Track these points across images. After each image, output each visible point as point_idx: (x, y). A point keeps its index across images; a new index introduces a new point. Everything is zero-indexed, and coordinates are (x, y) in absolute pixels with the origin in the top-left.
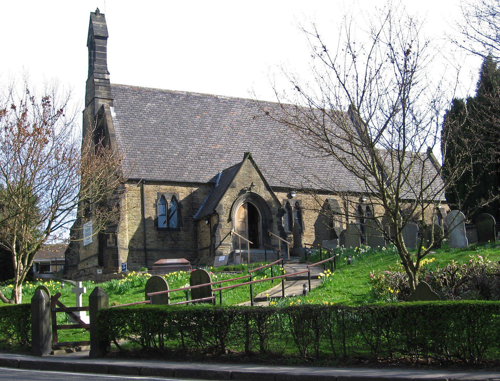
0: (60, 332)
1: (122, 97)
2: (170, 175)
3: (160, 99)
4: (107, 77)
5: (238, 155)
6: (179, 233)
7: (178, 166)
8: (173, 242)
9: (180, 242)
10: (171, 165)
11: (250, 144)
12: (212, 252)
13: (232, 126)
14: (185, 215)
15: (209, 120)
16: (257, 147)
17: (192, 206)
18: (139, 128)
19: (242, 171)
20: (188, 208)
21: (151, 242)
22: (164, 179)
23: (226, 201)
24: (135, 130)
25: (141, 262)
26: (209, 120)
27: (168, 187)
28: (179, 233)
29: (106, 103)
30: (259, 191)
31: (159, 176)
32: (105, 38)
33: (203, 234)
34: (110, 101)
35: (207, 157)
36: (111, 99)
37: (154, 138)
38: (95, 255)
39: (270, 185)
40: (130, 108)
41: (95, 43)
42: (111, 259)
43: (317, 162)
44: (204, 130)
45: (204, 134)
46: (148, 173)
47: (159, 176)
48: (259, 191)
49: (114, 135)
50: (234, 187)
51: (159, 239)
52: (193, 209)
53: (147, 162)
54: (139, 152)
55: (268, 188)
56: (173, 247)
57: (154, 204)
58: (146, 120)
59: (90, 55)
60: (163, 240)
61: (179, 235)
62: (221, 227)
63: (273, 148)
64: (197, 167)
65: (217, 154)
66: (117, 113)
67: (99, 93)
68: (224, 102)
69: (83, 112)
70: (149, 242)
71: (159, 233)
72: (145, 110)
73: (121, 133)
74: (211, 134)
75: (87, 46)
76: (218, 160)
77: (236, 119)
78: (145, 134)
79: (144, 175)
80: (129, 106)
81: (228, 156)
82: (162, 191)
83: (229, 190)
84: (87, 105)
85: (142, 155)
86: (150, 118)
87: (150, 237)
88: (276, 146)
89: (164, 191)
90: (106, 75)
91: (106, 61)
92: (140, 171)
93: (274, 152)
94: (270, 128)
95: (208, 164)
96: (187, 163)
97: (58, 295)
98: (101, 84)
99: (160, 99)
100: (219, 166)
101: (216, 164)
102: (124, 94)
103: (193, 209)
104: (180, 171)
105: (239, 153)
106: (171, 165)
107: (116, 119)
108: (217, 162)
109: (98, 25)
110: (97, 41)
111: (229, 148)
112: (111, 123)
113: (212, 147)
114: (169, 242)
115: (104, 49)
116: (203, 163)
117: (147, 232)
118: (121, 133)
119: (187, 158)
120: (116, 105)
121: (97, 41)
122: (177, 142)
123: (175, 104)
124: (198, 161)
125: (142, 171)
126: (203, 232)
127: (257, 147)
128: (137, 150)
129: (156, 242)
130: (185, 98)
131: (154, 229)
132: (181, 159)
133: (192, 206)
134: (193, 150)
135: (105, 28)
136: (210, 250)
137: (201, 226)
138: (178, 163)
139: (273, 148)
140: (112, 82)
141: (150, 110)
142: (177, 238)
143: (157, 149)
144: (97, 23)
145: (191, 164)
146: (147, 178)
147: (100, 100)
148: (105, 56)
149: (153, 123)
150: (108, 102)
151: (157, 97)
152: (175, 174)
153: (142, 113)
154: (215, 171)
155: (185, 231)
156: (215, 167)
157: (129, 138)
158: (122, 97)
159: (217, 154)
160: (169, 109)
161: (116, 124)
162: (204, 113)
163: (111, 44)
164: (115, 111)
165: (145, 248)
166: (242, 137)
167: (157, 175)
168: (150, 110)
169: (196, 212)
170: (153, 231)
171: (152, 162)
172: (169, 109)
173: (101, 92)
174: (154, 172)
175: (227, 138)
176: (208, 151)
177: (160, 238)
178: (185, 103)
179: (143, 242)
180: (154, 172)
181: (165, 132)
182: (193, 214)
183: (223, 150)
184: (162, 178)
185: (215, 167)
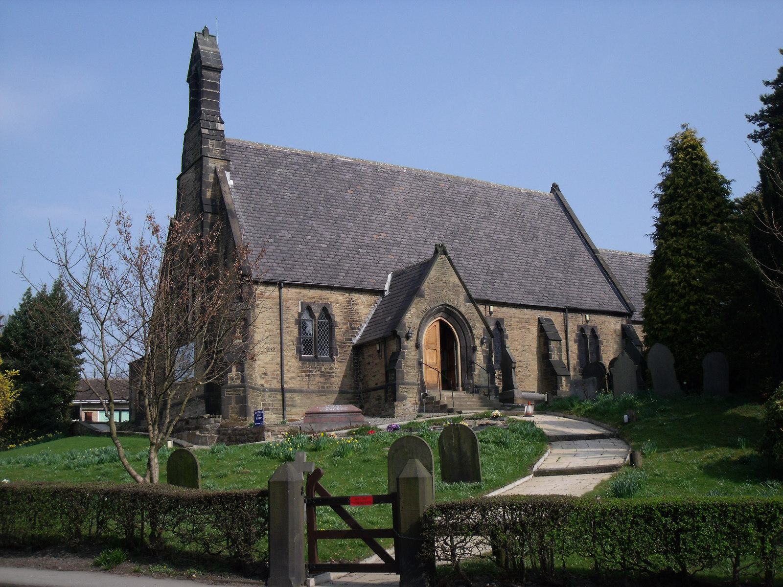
0: (321, 544)
1: (241, 158)
2: (319, 275)
3: (295, 164)
4: (220, 127)
5: (411, 250)
6: (333, 365)
7: (330, 263)
8: (322, 379)
9: (333, 380)
10: (319, 262)
11: (426, 234)
12: (389, 394)
13: (398, 207)
14: (341, 338)
15: (366, 197)
16: (436, 238)
17: (351, 324)
18: (268, 204)
19: (433, 273)
20: (345, 327)
21: (291, 379)
22: (311, 281)
23: (411, 317)
24: (264, 207)
25: (277, 409)
26: (366, 197)
27: (317, 293)
28: (333, 365)
29: (219, 165)
30: (457, 304)
31: (303, 277)
32: (219, 70)
33: (369, 367)
34: (225, 163)
35: (368, 251)
36: (227, 160)
37: (291, 219)
38: (200, 397)
39: (473, 296)
40: (254, 175)
41: (202, 76)
42: (233, 404)
43: (520, 264)
44: (359, 210)
45: (361, 216)
46: (287, 273)
47: (303, 277)
48: (457, 304)
49: (234, 216)
50: (422, 296)
51: (304, 374)
52: (353, 328)
53: (284, 255)
54: (272, 241)
55: (470, 299)
56: (323, 387)
57: (296, 320)
58: (278, 193)
59: (191, 94)
60: (309, 376)
61: (331, 368)
62: (404, 357)
63: (457, 241)
64: (355, 265)
65: (382, 246)
66: (236, 182)
67: (209, 150)
68: (384, 172)
69: (179, 179)
70: (287, 379)
71: (303, 364)
72: (275, 178)
73: (243, 210)
74: (371, 218)
75: (188, 81)
76: (385, 256)
77: (404, 197)
78: (278, 214)
79: (279, 272)
80: (252, 172)
81: (398, 251)
82: (308, 300)
83: (416, 300)
84: (185, 169)
85: (277, 244)
86: (282, 190)
87: (289, 371)
88: (462, 239)
89: (310, 301)
90: (219, 124)
91: (218, 104)
92: (275, 268)
93: (460, 248)
94: (450, 212)
95: (371, 261)
96: (341, 259)
97: (317, 474)
98: (211, 137)
99: (295, 164)
100: (388, 266)
101: (383, 262)
102: (243, 153)
103: (352, 328)
104: (332, 270)
105: (413, 247)
106: (319, 262)
107: (234, 190)
108: (384, 259)
109: (208, 51)
110: (202, 77)
111: (399, 239)
112: (229, 196)
113: (375, 236)
114: (318, 379)
115: (216, 86)
116: (364, 260)
117: (285, 362)
118: (243, 210)
119: (340, 251)
120: (233, 169)
121: (202, 77)
122: (324, 227)
123: (317, 172)
124: (356, 256)
125: (279, 268)
126: (369, 364)
127: (436, 238)
128: (268, 237)
129: (299, 379)
130: (330, 163)
131: (296, 358)
132: (332, 253)
133: (351, 324)
134: (347, 239)
135: (218, 55)
136: (386, 392)
137: (366, 355)
138: (328, 259)
139: (457, 241)
140: (228, 136)
141: (282, 179)
142: (328, 372)
143: (296, 236)
144: (206, 48)
145: (348, 261)
146: (286, 279)
147: (210, 160)
148: (217, 96)
149: (288, 198)
150: (223, 164)
151: (290, 160)
152: (326, 274)
153: (271, 183)
154: (382, 272)
155: (340, 362)
156: (382, 265)
157: (255, 219)
158: (241, 158)
159: (382, 246)
160: (308, 179)
161: (235, 197)
162: (358, 187)
163: (226, 81)
164: (232, 178)
165: (282, 388)
166: (414, 224)
167: (300, 274)
168: (282, 179)
169: (357, 333)
170: (294, 360)
171: (291, 256)
172: (308, 179)
173: (212, 147)
174: (295, 270)
175: (393, 224)
176: (369, 242)
177: (304, 371)
178: (330, 171)
179: (279, 377)
180: (295, 270)
181: (305, 212)
182: (352, 336)
183: (391, 241)
184: (308, 281)
185: (382, 265)
